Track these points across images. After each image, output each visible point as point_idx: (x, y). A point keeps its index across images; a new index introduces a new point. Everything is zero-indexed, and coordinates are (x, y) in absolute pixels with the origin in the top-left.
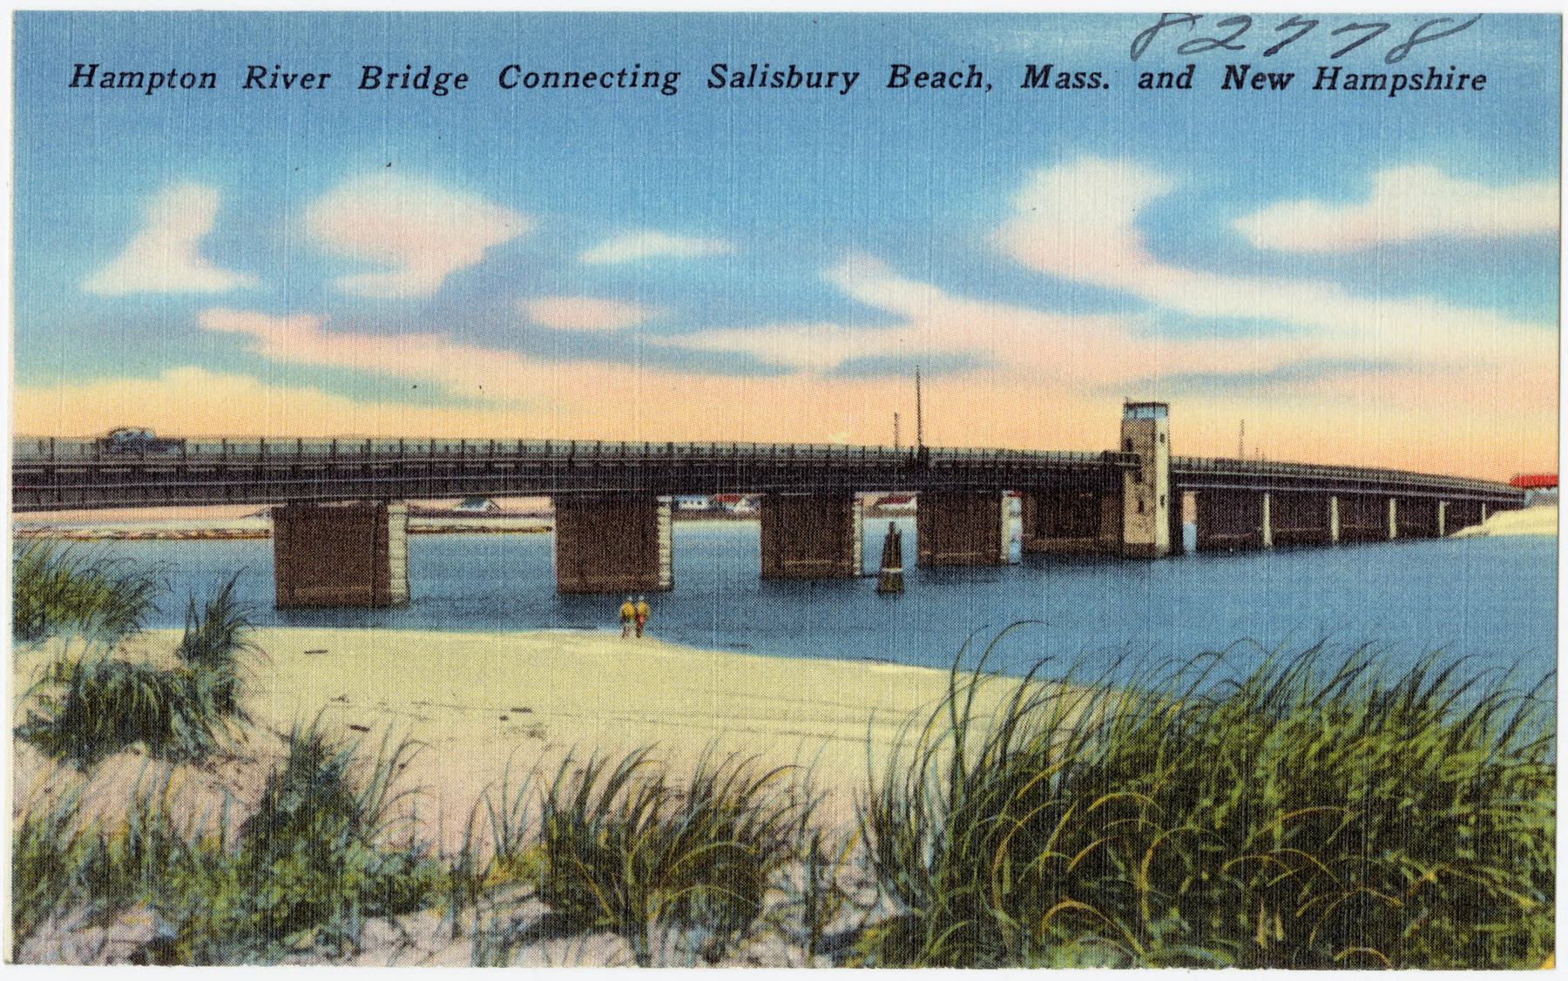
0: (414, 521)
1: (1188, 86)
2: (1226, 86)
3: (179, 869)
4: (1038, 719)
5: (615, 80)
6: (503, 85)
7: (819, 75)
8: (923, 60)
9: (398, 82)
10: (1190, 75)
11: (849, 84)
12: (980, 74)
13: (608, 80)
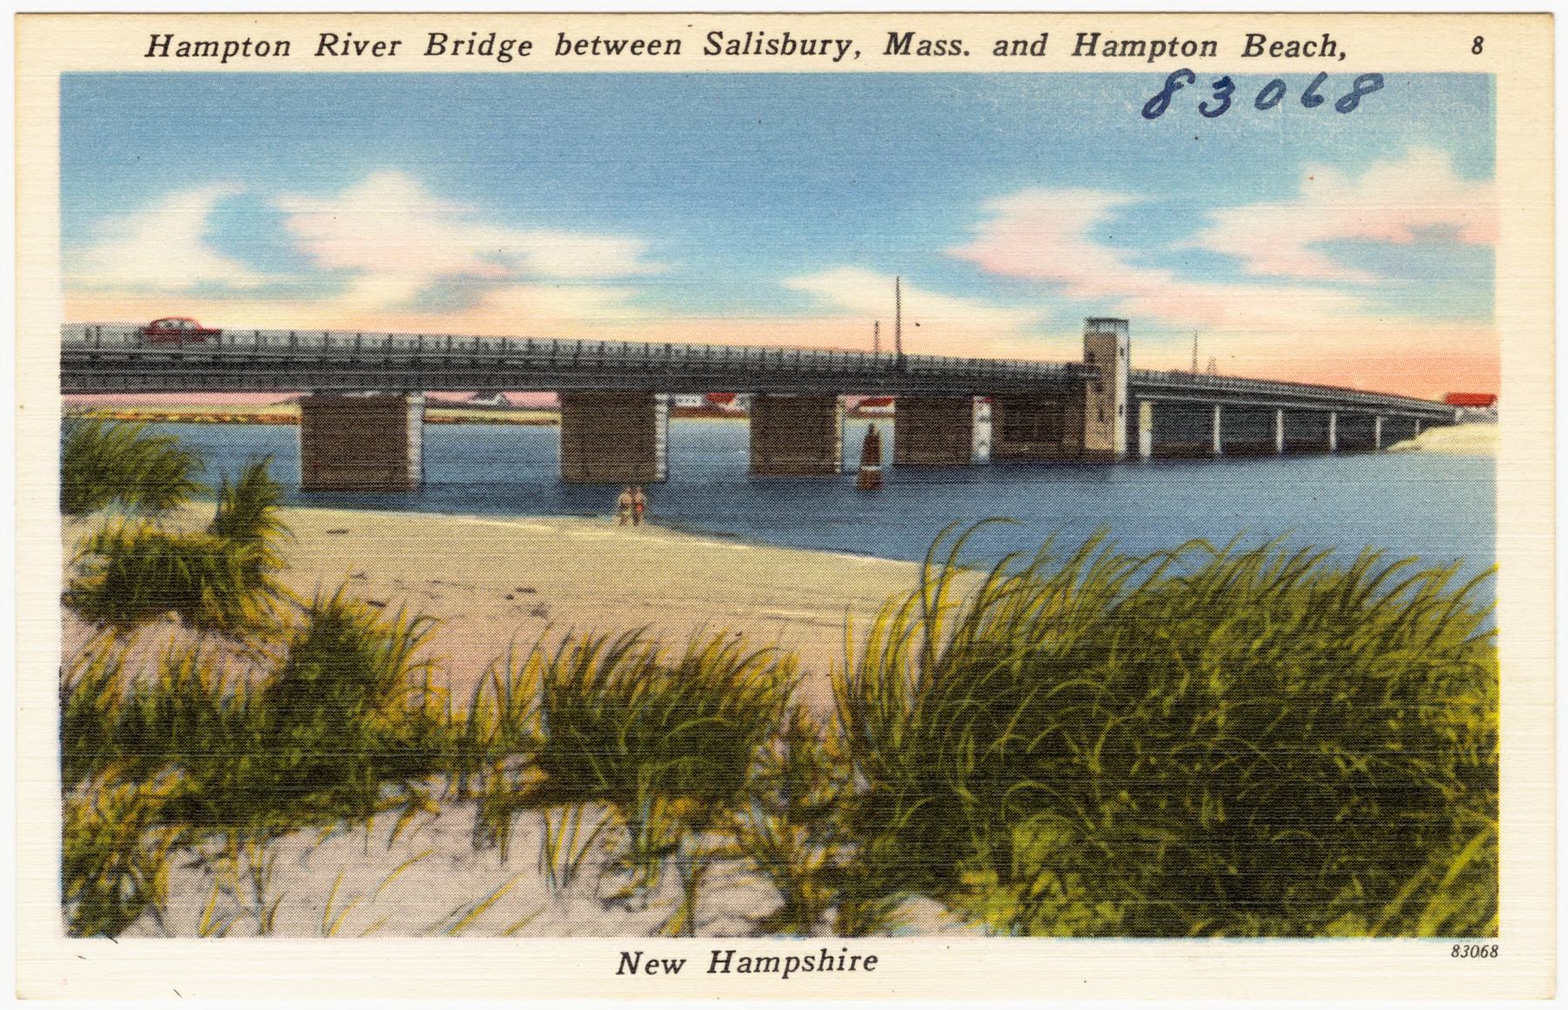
0: (431, 412)
12: (1334, 44)
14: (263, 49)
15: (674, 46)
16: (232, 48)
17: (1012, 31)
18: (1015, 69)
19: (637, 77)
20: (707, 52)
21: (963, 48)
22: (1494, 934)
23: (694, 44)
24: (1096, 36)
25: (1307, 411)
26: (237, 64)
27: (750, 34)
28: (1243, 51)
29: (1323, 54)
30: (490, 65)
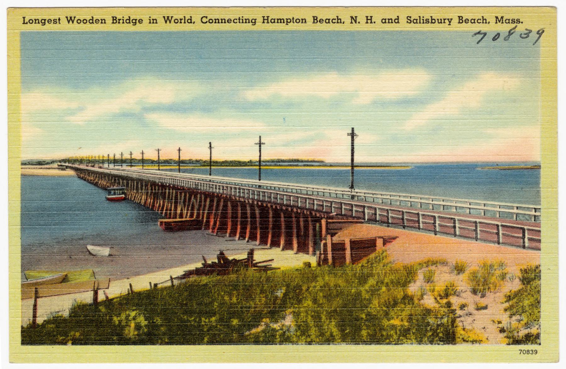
0: (216, 200)
1: (398, 22)
2: (496, 23)
3: (367, 297)
4: (124, 290)
5: (238, 21)
6: (203, 23)
7: (441, 20)
8: (273, 15)
9: (121, 21)
10: (398, 19)
11: (450, 22)
12: (486, 20)
13: (235, 21)
14: (298, 21)
15: (304, 21)
16: (288, 21)
18: (243, 29)
24: (268, 17)
25: (491, 224)
27: (420, 17)
29: (483, 23)
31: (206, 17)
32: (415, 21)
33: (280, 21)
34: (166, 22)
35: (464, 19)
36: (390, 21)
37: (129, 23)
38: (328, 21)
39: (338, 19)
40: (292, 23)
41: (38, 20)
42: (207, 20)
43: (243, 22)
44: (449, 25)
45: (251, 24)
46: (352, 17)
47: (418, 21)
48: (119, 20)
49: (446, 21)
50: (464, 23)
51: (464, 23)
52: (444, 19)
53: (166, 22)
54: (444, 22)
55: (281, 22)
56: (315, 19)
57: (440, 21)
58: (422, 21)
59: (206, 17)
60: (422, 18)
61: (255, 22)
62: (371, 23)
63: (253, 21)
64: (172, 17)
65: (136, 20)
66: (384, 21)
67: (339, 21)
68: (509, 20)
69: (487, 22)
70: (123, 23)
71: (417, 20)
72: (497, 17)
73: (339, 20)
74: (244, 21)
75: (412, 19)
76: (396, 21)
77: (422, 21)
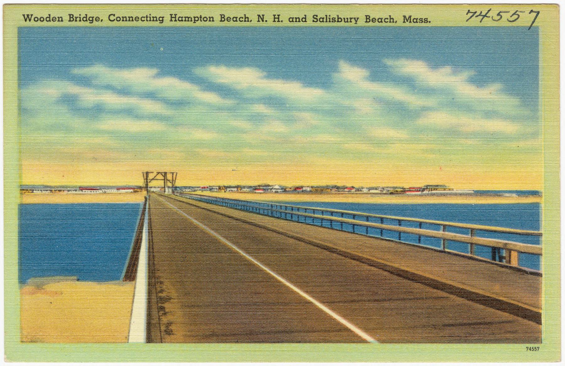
5: (145, 19)
6: (111, 21)
8: (38, 14)
9: (78, 19)
14: (205, 19)
16: (196, 19)
17: (295, 14)
19: (141, 28)
20: (313, 21)
21: (429, 20)
22: (156, 331)
23: (217, 18)
24: (176, 15)
26: (199, 24)
27: (326, 16)
28: (69, 19)
30: (87, 24)
31: (114, 15)
32: (322, 20)
33: (188, 19)
34: (26, 20)
35: (371, 19)
36: (297, 19)
37: (86, 20)
38: (235, 19)
39: (390, 19)
40: (199, 21)
41: (299, 18)
42: (115, 18)
43: (150, 20)
44: (356, 23)
45: (89, 21)
46: (259, 16)
47: (325, 20)
48: (76, 18)
49: (353, 20)
50: (226, 21)
51: (226, 21)
52: (351, 19)
53: (26, 20)
54: (351, 22)
55: (188, 21)
56: (222, 17)
57: (346, 20)
58: (328, 20)
59: (114, 15)
60: (328, 17)
61: (163, 20)
62: (279, 21)
63: (91, 19)
64: (32, 15)
65: (93, 17)
66: (291, 20)
67: (392, 20)
68: (417, 19)
69: (395, 21)
70: (80, 21)
71: (323, 18)
72: (405, 17)
73: (246, 19)
74: (152, 19)
75: (318, 18)
76: (304, 20)
77: (328, 20)
